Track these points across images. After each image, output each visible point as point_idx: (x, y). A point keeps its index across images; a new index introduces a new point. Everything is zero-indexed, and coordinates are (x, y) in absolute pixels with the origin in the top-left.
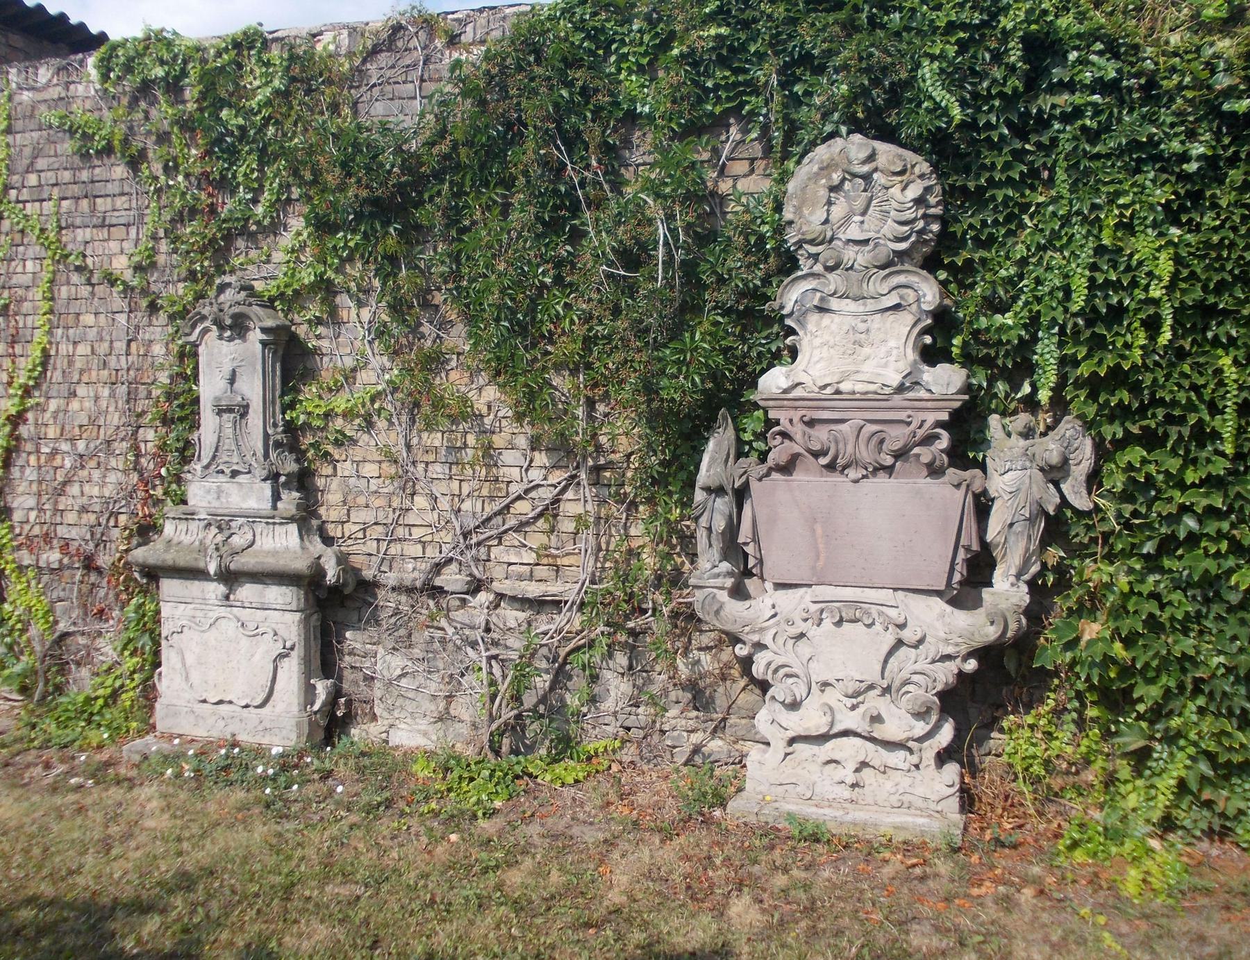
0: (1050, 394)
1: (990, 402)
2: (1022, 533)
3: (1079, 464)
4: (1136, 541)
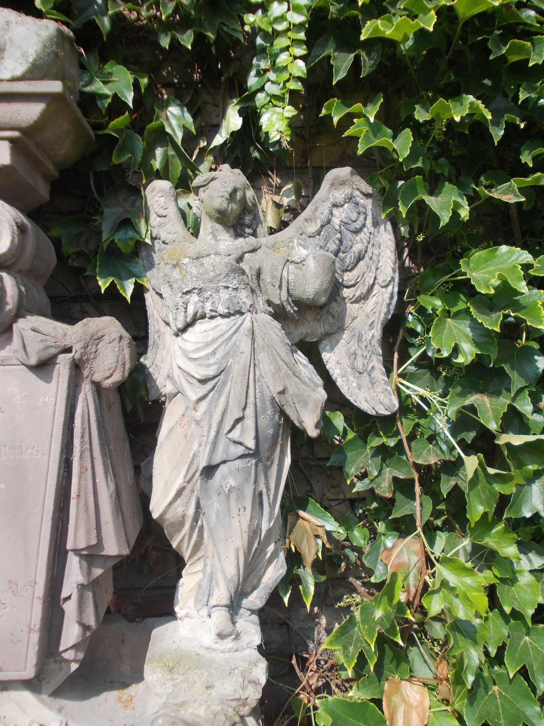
0: (290, 111)
1: (149, 153)
2: (239, 490)
3: (364, 297)
4: (509, 489)
